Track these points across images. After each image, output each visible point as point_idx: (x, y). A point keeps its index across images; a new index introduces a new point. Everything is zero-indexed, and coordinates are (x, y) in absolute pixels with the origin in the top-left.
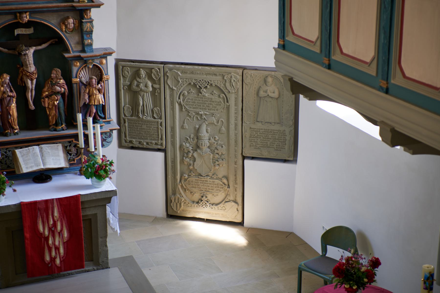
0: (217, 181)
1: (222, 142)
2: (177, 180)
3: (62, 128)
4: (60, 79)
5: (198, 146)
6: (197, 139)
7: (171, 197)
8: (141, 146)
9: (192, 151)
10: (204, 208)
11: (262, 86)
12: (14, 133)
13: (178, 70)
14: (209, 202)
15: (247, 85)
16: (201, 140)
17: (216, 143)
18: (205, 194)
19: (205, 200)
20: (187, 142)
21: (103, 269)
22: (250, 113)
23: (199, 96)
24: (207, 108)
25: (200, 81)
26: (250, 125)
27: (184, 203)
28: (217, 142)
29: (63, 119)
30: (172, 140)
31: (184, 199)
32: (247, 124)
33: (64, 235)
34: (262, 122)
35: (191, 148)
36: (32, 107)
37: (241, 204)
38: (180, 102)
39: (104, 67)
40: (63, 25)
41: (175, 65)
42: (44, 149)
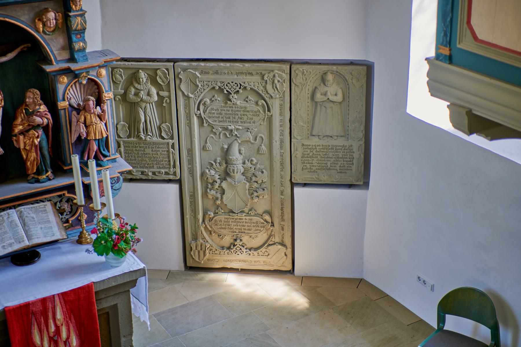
0: (255, 219)
1: (262, 166)
2: (199, 220)
3: (47, 177)
4: (40, 105)
5: (228, 172)
6: (226, 163)
8: (144, 177)
9: (219, 180)
10: (238, 254)
11: (318, 87)
13: (195, 69)
14: (245, 247)
16: (232, 164)
17: (253, 167)
18: (239, 236)
19: (239, 244)
20: (211, 168)
22: (302, 124)
23: (227, 105)
25: (229, 83)
26: (301, 140)
27: (209, 250)
28: (254, 167)
29: (47, 163)
30: (190, 166)
31: (209, 245)
32: (297, 139)
33: (72, 343)
34: (319, 136)
37: (291, 247)
38: (200, 114)
39: (104, 81)
40: (39, 22)
41: (190, 63)
42: (25, 213)
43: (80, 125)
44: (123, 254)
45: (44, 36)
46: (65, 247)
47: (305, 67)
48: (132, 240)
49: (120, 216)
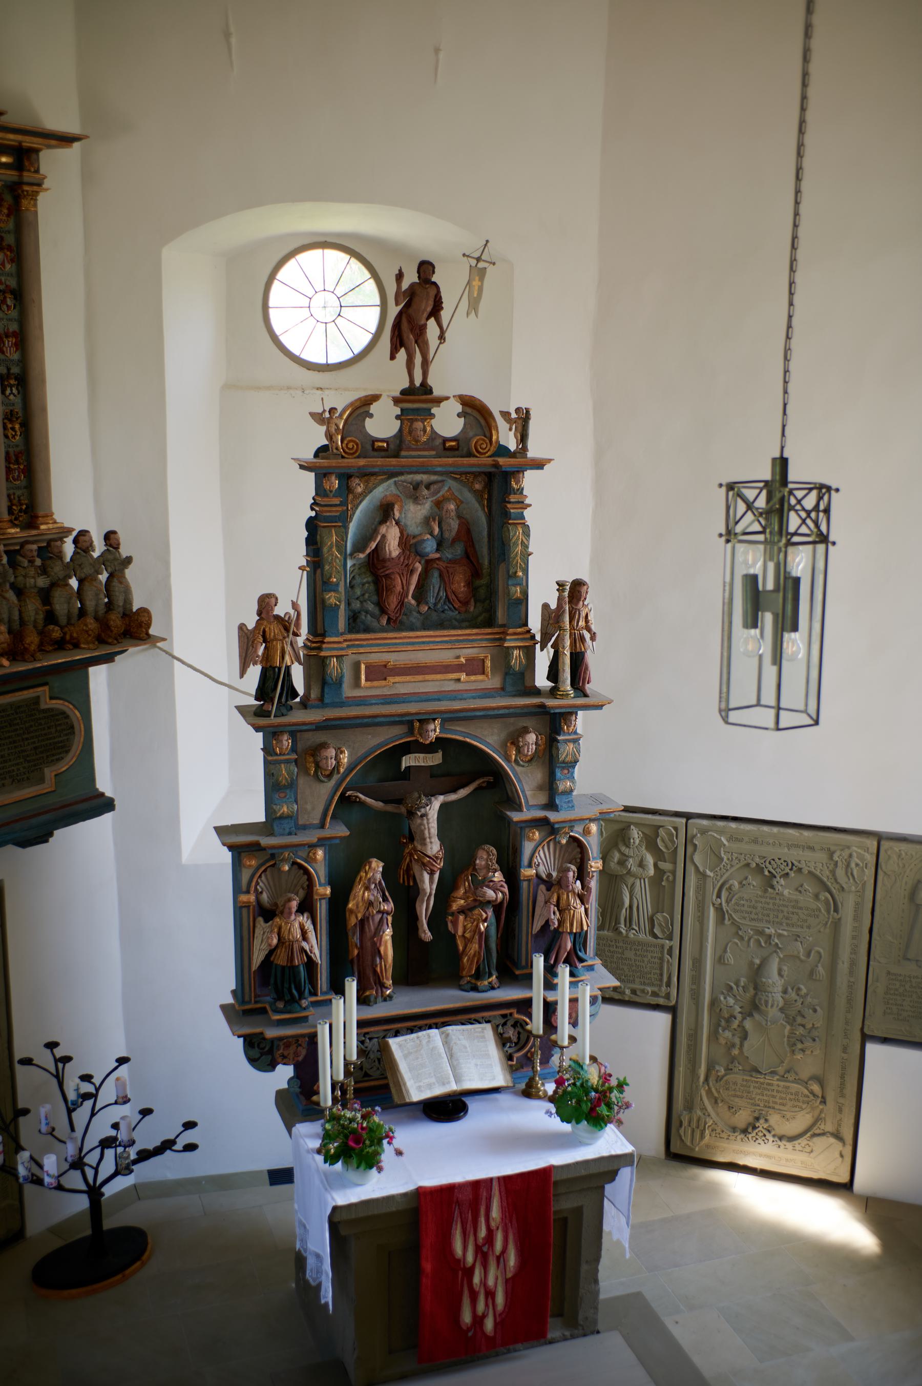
0: (795, 1087)
2: (699, 1078)
3: (490, 983)
4: (495, 871)
6: (756, 988)
7: (682, 1115)
9: (740, 1015)
10: (760, 1144)
12: (385, 996)
13: (721, 832)
14: (773, 1133)
15: (889, 875)
16: (765, 992)
17: (800, 1001)
18: (763, 1112)
21: (585, 1335)
23: (767, 895)
24: (785, 921)
25: (773, 860)
27: (710, 1130)
28: (802, 1000)
30: (694, 987)
31: (711, 1122)
33: (508, 1261)
35: (738, 1009)
36: (427, 935)
38: (721, 904)
39: (592, 842)
40: (513, 746)
42: (454, 1037)
43: (550, 908)
44: (603, 1125)
45: (516, 767)
46: (504, 1099)
47: (903, 846)
48: (618, 1103)
49: (599, 1060)
